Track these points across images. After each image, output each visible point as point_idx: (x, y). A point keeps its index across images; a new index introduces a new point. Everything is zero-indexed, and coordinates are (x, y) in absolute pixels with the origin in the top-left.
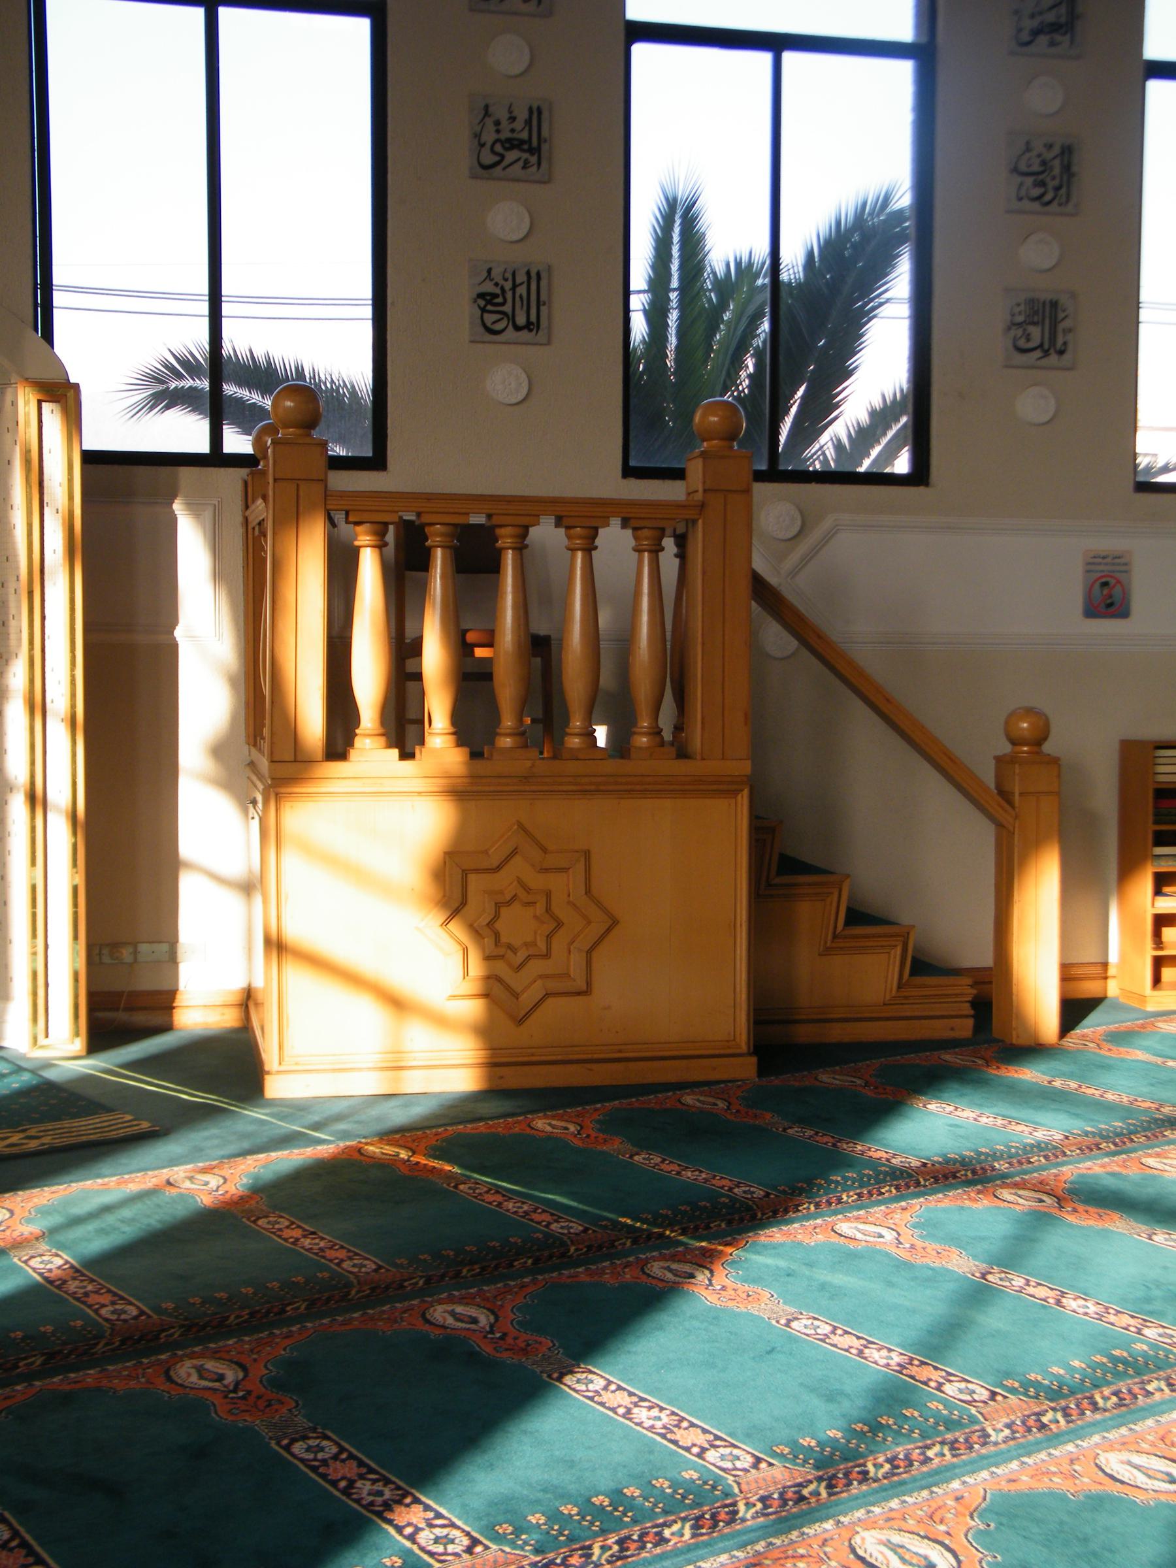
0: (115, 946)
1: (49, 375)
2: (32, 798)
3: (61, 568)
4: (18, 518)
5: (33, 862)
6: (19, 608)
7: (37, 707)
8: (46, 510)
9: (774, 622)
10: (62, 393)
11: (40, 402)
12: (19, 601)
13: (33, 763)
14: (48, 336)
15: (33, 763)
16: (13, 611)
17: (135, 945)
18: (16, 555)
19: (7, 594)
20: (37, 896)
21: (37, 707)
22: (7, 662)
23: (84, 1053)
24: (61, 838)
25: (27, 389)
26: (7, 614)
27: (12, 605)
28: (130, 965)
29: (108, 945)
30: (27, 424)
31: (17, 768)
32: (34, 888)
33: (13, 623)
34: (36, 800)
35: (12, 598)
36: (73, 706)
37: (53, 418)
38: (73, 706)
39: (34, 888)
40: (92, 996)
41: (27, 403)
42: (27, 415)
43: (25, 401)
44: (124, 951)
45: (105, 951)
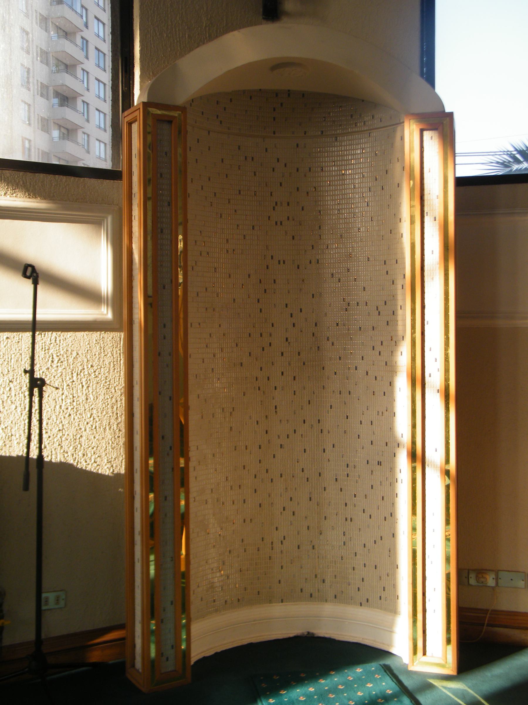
0: (480, 572)
1: (430, 109)
2: (413, 456)
3: (438, 271)
4: (405, 228)
5: (414, 513)
6: (404, 300)
7: (418, 381)
8: (426, 219)
9: (36, 161)
10: (441, 123)
11: (422, 131)
12: (404, 295)
13: (414, 426)
14: (429, 76)
15: (414, 426)
16: (400, 303)
17: (497, 572)
18: (404, 259)
19: (396, 289)
20: (419, 558)
21: (418, 381)
22: (396, 344)
23: (455, 673)
24: (436, 488)
25: (412, 122)
26: (396, 305)
27: (399, 297)
28: (493, 588)
29: (474, 570)
30: (411, 150)
31: (402, 427)
32: (414, 552)
33: (400, 312)
34: (418, 457)
35: (399, 292)
36: (447, 380)
37: (432, 144)
38: (447, 380)
39: (414, 552)
40: (460, 610)
41: (411, 134)
42: (411, 142)
43: (410, 131)
44: (487, 577)
45: (472, 576)
